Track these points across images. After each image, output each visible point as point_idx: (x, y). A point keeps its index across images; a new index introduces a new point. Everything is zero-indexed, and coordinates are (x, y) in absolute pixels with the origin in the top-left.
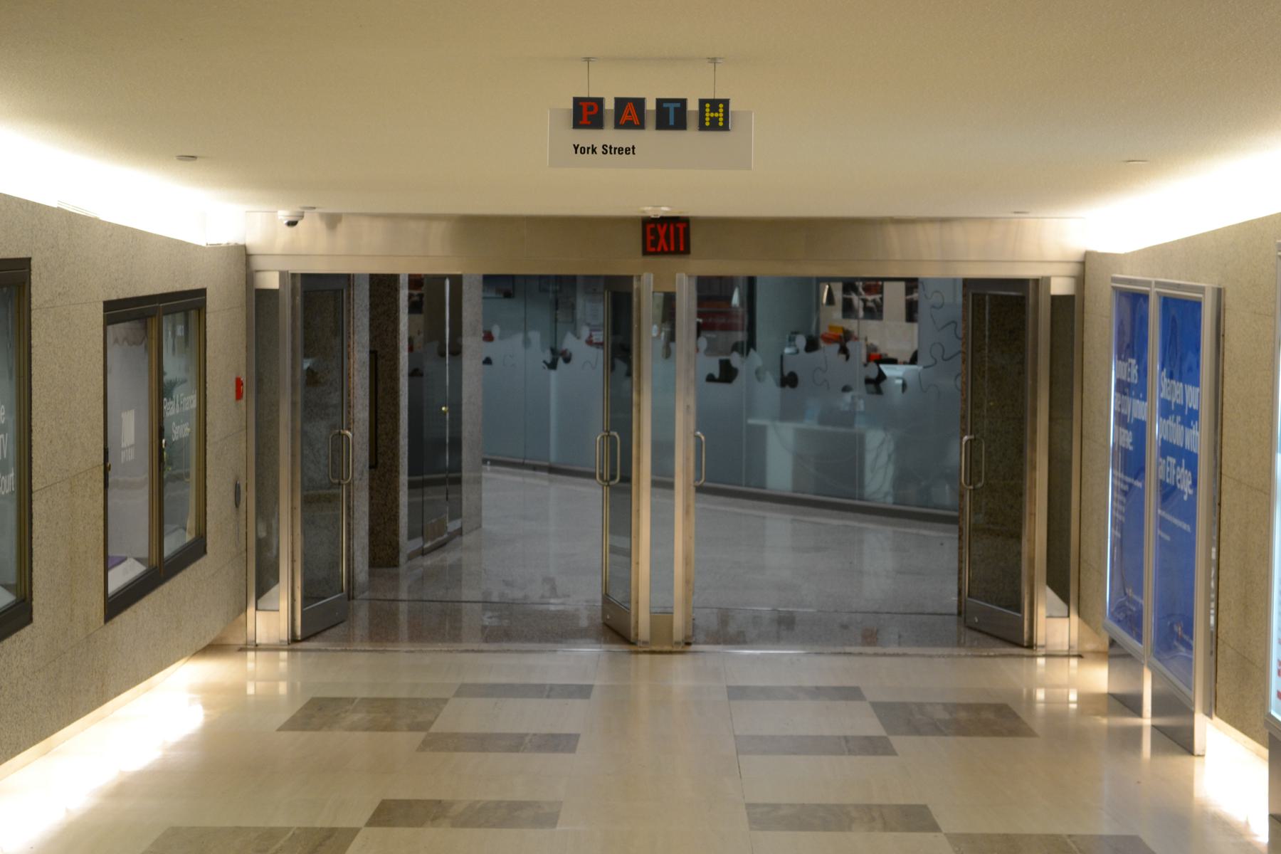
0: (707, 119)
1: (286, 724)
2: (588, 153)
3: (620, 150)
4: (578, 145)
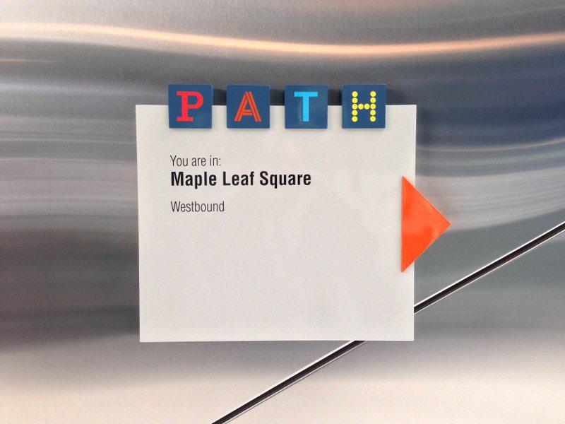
0: (355, 113)
1: (403, 261)
2: (299, 184)
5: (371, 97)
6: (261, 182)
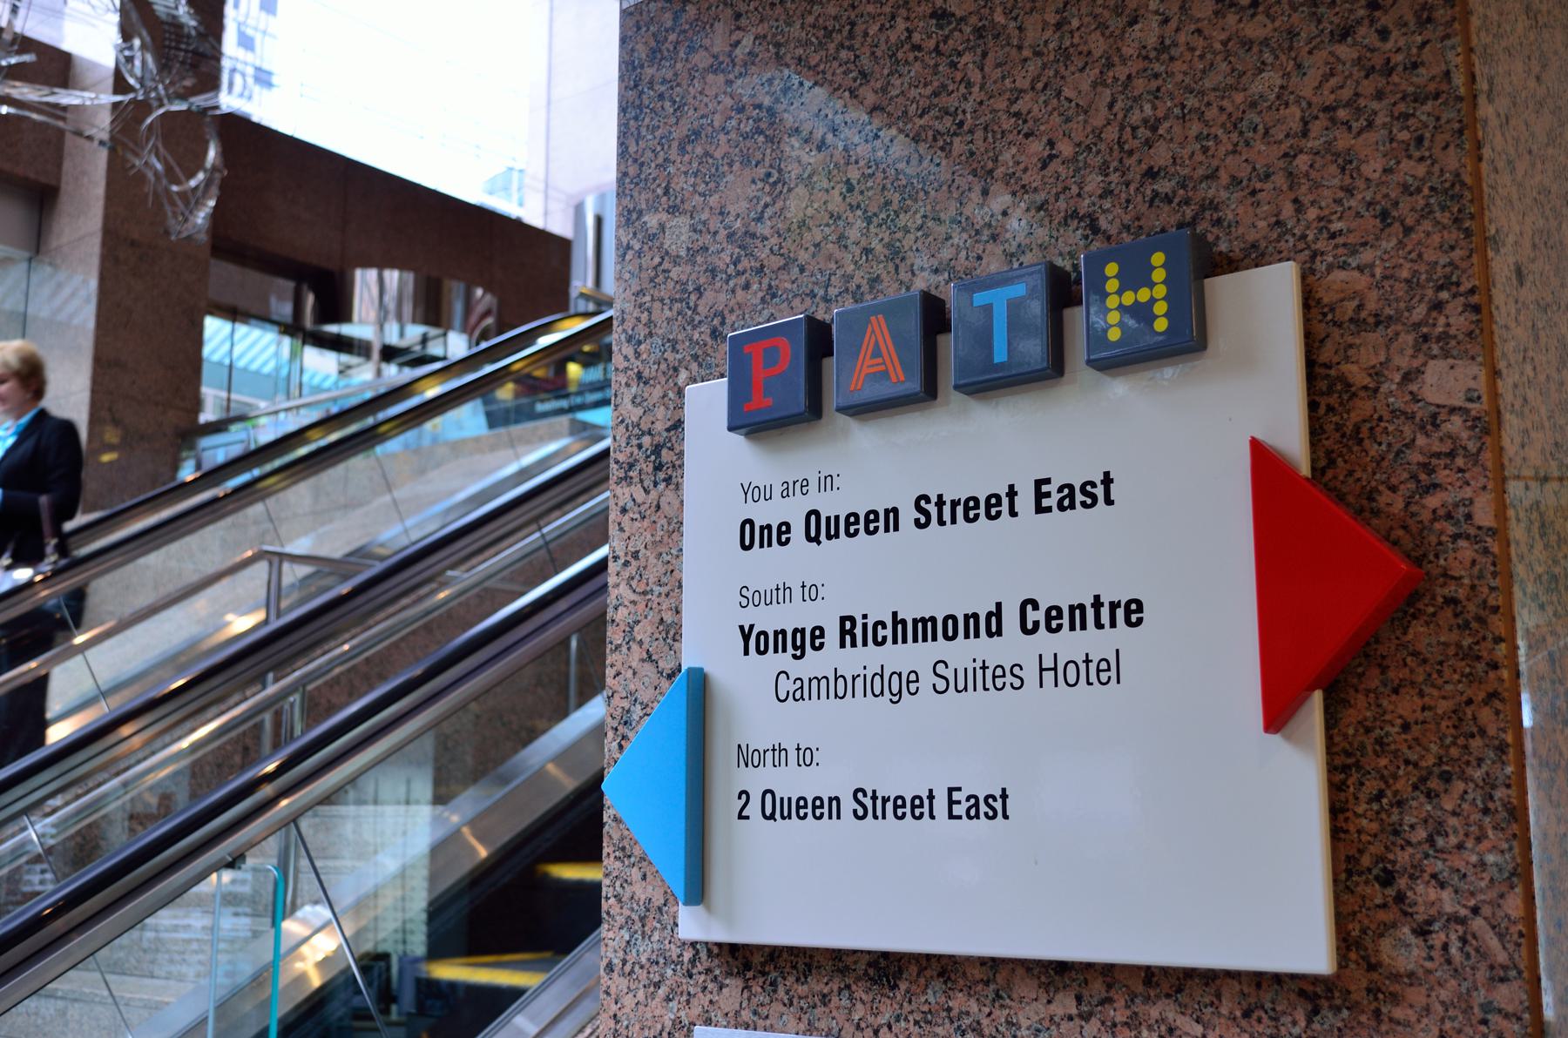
3: (969, 509)
4: (752, 627)
5: (1163, 266)
6: (855, 811)
